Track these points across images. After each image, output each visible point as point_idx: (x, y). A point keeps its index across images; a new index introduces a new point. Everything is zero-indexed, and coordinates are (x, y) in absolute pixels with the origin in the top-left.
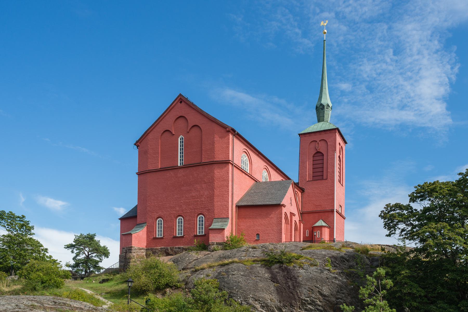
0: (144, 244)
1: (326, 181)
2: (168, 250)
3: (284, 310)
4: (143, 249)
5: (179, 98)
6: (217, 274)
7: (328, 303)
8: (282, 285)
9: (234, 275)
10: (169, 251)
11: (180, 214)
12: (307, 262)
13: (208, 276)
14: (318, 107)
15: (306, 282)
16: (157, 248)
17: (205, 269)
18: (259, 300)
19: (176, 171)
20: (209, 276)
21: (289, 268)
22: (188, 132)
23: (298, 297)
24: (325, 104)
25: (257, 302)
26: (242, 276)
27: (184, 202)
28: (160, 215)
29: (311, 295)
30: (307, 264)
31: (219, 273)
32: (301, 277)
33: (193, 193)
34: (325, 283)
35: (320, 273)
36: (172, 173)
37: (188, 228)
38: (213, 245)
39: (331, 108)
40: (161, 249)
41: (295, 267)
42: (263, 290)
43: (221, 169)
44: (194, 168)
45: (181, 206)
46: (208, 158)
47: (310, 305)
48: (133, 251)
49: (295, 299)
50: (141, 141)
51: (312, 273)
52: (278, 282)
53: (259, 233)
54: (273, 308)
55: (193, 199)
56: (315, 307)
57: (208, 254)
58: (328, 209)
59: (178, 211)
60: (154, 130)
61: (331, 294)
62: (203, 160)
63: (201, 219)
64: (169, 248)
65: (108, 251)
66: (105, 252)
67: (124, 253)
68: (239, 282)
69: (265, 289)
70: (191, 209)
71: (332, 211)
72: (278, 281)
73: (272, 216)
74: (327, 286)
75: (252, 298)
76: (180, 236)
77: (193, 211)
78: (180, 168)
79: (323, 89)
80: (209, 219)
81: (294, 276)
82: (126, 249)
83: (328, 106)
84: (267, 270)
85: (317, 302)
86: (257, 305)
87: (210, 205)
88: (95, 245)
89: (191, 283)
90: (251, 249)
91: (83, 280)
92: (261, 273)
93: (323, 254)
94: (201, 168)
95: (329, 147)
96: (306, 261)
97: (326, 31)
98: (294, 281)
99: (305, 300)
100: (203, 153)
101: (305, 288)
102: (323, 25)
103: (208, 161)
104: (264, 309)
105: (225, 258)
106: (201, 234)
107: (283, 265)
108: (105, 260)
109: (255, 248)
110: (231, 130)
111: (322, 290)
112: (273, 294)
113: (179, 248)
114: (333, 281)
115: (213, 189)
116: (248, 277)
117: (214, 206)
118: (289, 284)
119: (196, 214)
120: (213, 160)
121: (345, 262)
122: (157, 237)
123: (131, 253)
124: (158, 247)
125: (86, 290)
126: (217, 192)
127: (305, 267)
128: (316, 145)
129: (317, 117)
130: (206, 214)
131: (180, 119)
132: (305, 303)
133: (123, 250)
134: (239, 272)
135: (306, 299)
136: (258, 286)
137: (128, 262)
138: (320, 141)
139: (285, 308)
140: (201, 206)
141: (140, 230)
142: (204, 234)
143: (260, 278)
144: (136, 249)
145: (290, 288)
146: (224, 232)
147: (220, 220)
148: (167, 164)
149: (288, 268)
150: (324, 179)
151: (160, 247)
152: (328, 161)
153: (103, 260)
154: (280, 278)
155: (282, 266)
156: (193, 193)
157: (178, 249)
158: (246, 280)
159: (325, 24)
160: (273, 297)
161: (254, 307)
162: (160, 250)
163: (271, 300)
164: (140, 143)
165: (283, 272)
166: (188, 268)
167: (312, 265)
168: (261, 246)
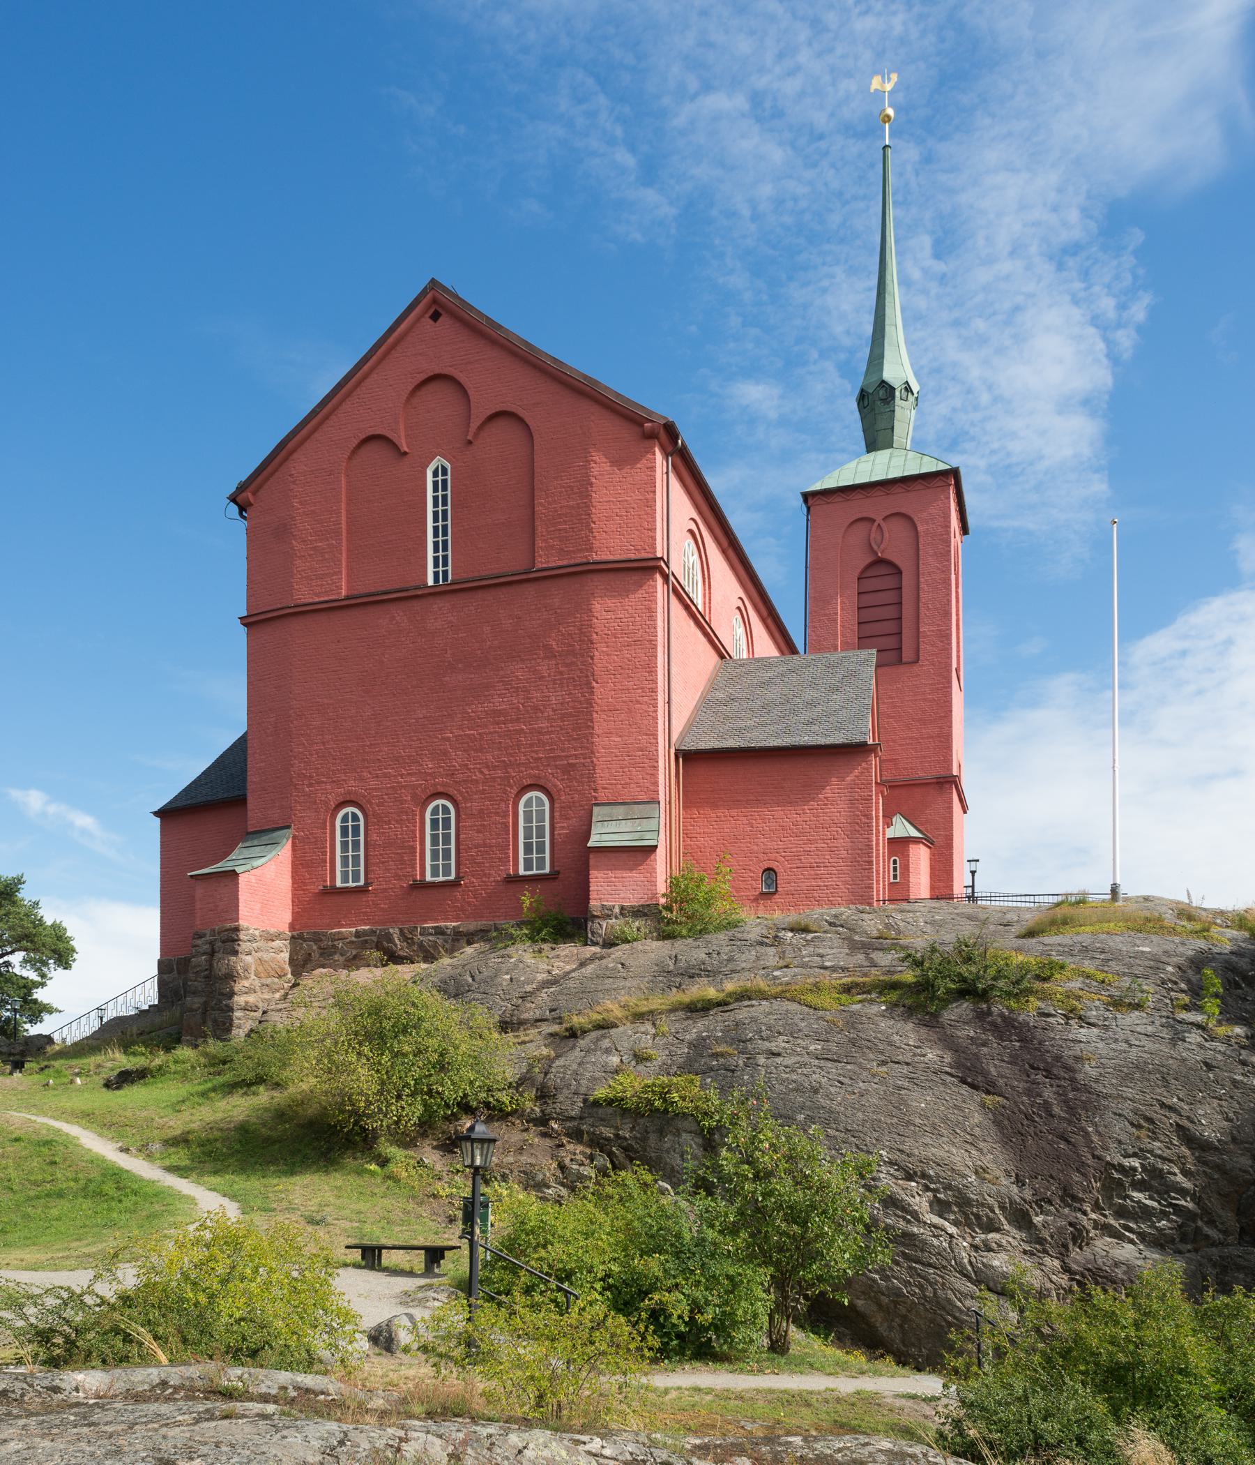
0: (282, 918)
1: (915, 669)
2: (390, 940)
3: (1038, 1219)
4: (278, 936)
5: (429, 296)
6: (686, 1050)
7: (1216, 1177)
8: (1015, 1102)
9: (779, 1055)
10: (396, 945)
11: (440, 789)
12: (1093, 989)
13: (640, 1058)
14: (868, 393)
15: (1122, 1086)
16: (339, 932)
17: (616, 1026)
18: (924, 1175)
19: (417, 605)
20: (647, 1059)
21: (1021, 1019)
22: (470, 442)
23: (1094, 1156)
24: (897, 384)
25: (913, 1184)
26: (818, 1059)
27: (456, 736)
28: (350, 792)
29: (1146, 1143)
30: (1099, 1000)
31: (699, 1046)
32: (1093, 1064)
33: (496, 699)
34: (1201, 1085)
35: (1173, 1042)
36: (399, 614)
37: (477, 846)
38: (609, 917)
39: (917, 399)
40: (358, 934)
41: (1049, 1015)
42: (933, 1126)
43: (620, 595)
44: (502, 594)
45: (445, 753)
46: (562, 549)
47: (1140, 1191)
48: (244, 946)
49: (1081, 1168)
50: (260, 486)
51: (1137, 1043)
52: (990, 1088)
53: (774, 865)
54: (993, 1211)
55: (498, 724)
56: (1166, 1200)
57: (593, 958)
58: (921, 774)
59: (430, 774)
60: (316, 435)
61: (1234, 1139)
62: (538, 560)
63: (441, 816)
64: (394, 931)
65: (68, 942)
66: (61, 946)
67: (204, 954)
68: (816, 1091)
69: (945, 1120)
70: (488, 767)
71: (937, 783)
72: (993, 1084)
73: (828, 792)
74: (1216, 1102)
75: (891, 1163)
76: (441, 879)
77: (499, 773)
78: (436, 593)
79: (887, 328)
80: (570, 808)
81: (1058, 1058)
82: (208, 938)
83: (908, 389)
84: (923, 1030)
85: (1172, 1177)
86: (917, 1198)
87: (575, 749)
88: (22, 920)
89: (565, 1091)
90: (790, 934)
91: (21, 1072)
92: (903, 1046)
93: (1142, 952)
94: (530, 590)
95: (921, 540)
96: (1086, 988)
97: (890, 112)
98: (1062, 1083)
99: (1121, 1168)
100: (540, 529)
101: (1120, 1115)
102: (879, 87)
103: (560, 563)
104: (946, 1216)
105: (692, 974)
106: (535, 872)
107: (989, 1008)
108: (57, 975)
109: (805, 930)
110: (662, 432)
111: (1192, 1122)
112: (981, 1145)
113: (439, 932)
114: (1239, 1078)
115: (586, 682)
116: (849, 1067)
117: (592, 752)
118: (1046, 1094)
119: (511, 787)
120: (586, 557)
121: (1241, 988)
122: (339, 884)
123: (236, 953)
124: (342, 926)
125: (73, 1130)
126: (603, 693)
127: (1094, 1013)
128: (873, 536)
129: (864, 431)
130: (555, 786)
131: (432, 387)
132: (1120, 1183)
133: (199, 942)
134: (799, 1041)
135: (1127, 1162)
136: (907, 1105)
137: (223, 994)
138: (885, 519)
139: (1041, 1207)
140: (536, 752)
141: (269, 857)
142: (547, 870)
143: (905, 1070)
144: (253, 939)
145: (1053, 1116)
146: (655, 860)
147: (620, 811)
148: (375, 580)
149: (1015, 1020)
150: (904, 660)
151: (354, 930)
152: (922, 595)
153: (51, 978)
154: (995, 1066)
155: (989, 1013)
156: (496, 699)
157: (436, 934)
158: (846, 1081)
159: (888, 87)
160: (987, 1161)
161: (904, 1209)
162: (354, 939)
163: (976, 1173)
164: (254, 494)
165: (1003, 1041)
166: (521, 1023)
167: (1117, 1003)
168: (826, 921)
